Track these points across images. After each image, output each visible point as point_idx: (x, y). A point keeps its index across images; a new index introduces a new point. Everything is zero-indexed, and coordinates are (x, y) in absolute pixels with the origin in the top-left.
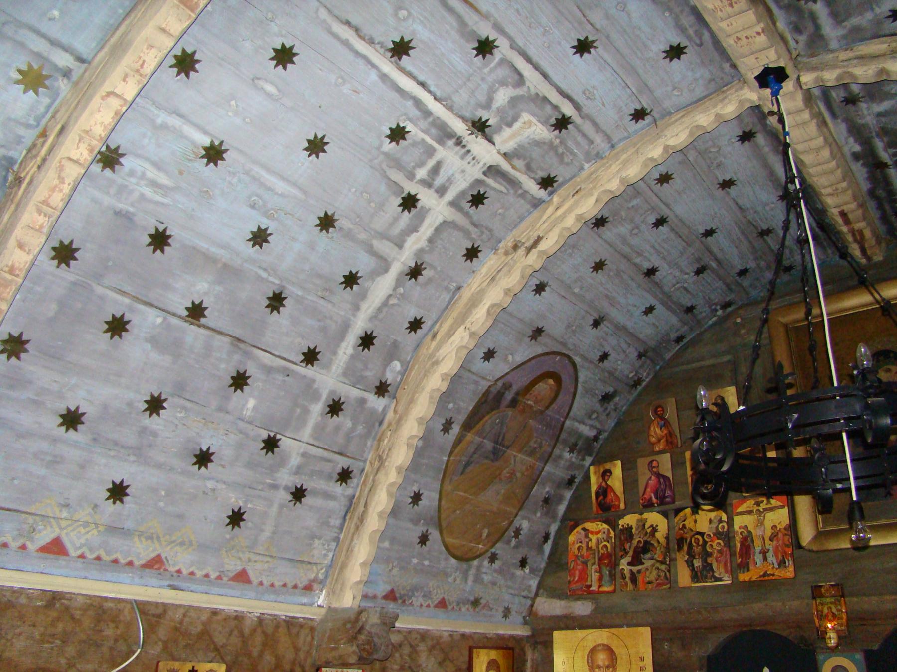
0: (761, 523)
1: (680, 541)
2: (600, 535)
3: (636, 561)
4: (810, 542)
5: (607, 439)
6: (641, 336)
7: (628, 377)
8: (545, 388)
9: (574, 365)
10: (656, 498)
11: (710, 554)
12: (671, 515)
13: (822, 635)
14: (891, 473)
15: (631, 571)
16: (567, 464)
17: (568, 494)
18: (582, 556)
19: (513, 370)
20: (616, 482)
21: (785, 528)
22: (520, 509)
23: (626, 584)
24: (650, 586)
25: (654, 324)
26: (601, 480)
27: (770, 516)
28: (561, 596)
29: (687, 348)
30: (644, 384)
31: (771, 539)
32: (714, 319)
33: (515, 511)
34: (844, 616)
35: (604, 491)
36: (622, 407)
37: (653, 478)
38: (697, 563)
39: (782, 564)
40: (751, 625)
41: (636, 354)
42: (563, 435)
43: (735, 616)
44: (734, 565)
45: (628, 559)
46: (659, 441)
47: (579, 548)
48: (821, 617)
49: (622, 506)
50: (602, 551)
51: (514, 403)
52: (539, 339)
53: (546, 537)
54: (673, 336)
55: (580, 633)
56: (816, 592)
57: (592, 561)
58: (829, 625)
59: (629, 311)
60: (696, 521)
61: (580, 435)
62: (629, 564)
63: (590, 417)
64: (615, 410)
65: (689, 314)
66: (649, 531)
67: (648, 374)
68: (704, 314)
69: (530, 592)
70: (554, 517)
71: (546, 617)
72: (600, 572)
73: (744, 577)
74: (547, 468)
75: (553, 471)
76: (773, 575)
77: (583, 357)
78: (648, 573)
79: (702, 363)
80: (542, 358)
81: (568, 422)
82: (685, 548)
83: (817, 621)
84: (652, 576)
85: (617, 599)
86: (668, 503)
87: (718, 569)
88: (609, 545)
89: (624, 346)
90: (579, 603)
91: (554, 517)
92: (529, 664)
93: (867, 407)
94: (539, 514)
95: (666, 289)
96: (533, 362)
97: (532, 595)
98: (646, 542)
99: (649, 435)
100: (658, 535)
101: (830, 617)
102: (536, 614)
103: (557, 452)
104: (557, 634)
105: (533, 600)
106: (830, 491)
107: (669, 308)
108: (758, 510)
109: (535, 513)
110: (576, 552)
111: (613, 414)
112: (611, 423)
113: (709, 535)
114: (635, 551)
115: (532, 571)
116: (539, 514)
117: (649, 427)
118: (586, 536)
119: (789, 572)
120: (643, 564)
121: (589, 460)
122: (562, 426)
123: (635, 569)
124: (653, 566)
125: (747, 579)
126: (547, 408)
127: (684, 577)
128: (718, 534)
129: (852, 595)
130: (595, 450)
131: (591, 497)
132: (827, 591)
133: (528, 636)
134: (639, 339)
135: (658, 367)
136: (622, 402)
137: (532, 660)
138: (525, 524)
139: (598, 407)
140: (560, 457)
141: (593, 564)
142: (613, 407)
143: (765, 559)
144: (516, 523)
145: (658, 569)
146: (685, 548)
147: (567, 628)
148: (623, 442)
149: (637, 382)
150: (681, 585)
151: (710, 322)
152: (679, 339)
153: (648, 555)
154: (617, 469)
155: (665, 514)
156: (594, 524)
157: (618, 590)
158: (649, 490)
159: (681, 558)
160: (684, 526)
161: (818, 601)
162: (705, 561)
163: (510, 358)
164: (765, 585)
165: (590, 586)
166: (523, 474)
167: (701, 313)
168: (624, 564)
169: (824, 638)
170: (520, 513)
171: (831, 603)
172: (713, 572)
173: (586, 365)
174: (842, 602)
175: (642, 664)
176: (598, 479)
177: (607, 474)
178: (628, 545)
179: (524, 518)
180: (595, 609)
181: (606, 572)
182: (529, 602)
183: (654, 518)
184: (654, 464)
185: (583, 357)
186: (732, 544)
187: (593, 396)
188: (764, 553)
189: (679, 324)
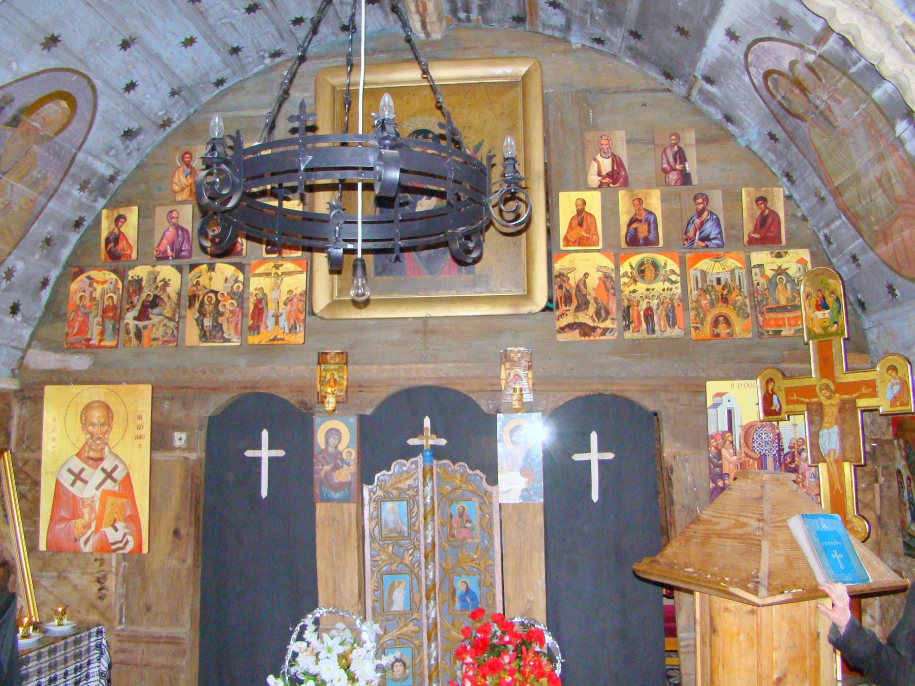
0: (277, 287)
1: (192, 298)
2: (106, 286)
3: (143, 315)
4: (322, 310)
5: (125, 181)
6: (177, 71)
7: (156, 114)
8: (56, 110)
9: (94, 89)
10: (172, 250)
11: (221, 314)
12: (186, 269)
13: (322, 400)
14: (401, 239)
15: (137, 325)
16: (77, 203)
17: (74, 238)
18: (84, 306)
19: (18, 81)
20: (130, 229)
21: (301, 294)
22: (15, 247)
23: (130, 340)
24: (155, 343)
25: (193, 59)
26: (114, 226)
27: (287, 280)
28: (58, 349)
29: (227, 94)
30: (174, 126)
31: (285, 304)
32: (261, 67)
33: (9, 250)
34: (345, 383)
35: (115, 239)
36: (147, 148)
37: (171, 229)
38: (208, 322)
39: (293, 329)
40: (254, 387)
41: (169, 90)
42: (73, 169)
43: (240, 378)
44: (245, 328)
45: (135, 313)
46: (183, 190)
47: (81, 298)
48: (323, 382)
49: (134, 256)
50: (106, 303)
51: (15, 122)
52: (53, 49)
53: (45, 283)
54: (213, 78)
55: (74, 389)
56: (322, 358)
57: (94, 312)
58: (329, 390)
59: (165, 38)
60: (211, 279)
61: (94, 173)
62: (135, 319)
63: (107, 153)
64: (138, 150)
65: (234, 56)
66: (160, 284)
67: (180, 116)
68: (250, 59)
69: (20, 342)
70: (55, 262)
71: (38, 370)
72: (103, 324)
73: (253, 339)
74: (50, 204)
75: (57, 208)
76: (283, 340)
77: (105, 82)
78: (154, 329)
79: (240, 113)
80: (52, 74)
81: (81, 156)
82: (197, 305)
83: (318, 385)
84: (159, 333)
85: (119, 354)
86: (185, 257)
87: (229, 329)
88: (115, 297)
89: (156, 78)
90: (77, 357)
91: (55, 262)
92: (15, 421)
93: (381, 157)
94: (37, 256)
95: (212, 21)
96: (44, 76)
97: (24, 346)
98: (156, 297)
99: (172, 183)
100: (169, 290)
101: (332, 383)
102: (27, 368)
103: (65, 187)
104: (48, 389)
105: (25, 351)
106: (341, 251)
107: (211, 44)
108: (276, 273)
109: (33, 254)
110: (78, 302)
111: (135, 154)
112: (131, 165)
113: (223, 294)
114: (143, 305)
115: (26, 320)
116: (37, 256)
117: (174, 174)
118: (91, 285)
119: (299, 338)
120: (150, 319)
121: (102, 202)
122: (73, 159)
123: (141, 324)
124: (160, 322)
125: (256, 342)
126: (57, 134)
127: (192, 334)
128: (232, 295)
129: (355, 364)
130: (111, 192)
131: (100, 243)
132: (332, 358)
133: (16, 391)
134: (173, 74)
135: (192, 110)
136: (148, 141)
137: (20, 417)
138: (20, 266)
139: (118, 143)
140: (68, 194)
141: (96, 316)
142: (135, 146)
143: (277, 323)
144: (9, 263)
145: (165, 325)
146: (197, 305)
147: (61, 382)
148: (143, 187)
149: (166, 124)
150: (188, 344)
151: (256, 70)
152: (220, 83)
153: (157, 310)
154: (133, 215)
155: (179, 269)
156: (101, 273)
157: (120, 346)
158: (165, 241)
159: (191, 315)
160: (198, 283)
161: (323, 366)
162: (215, 320)
163: (14, 66)
164: (273, 348)
165: (90, 340)
166: (21, 208)
167: (247, 57)
168: (129, 319)
169: (323, 402)
170: (15, 252)
171: (335, 370)
172: (223, 332)
173: (108, 91)
174: (345, 370)
175: (139, 422)
176: (109, 225)
177: (120, 219)
178: (135, 299)
179: (22, 259)
180: (94, 364)
181: (109, 325)
182: (20, 354)
183: (167, 271)
184: (174, 214)
185: (105, 82)
186: (245, 305)
187: (113, 130)
188: (277, 317)
189: (221, 66)
